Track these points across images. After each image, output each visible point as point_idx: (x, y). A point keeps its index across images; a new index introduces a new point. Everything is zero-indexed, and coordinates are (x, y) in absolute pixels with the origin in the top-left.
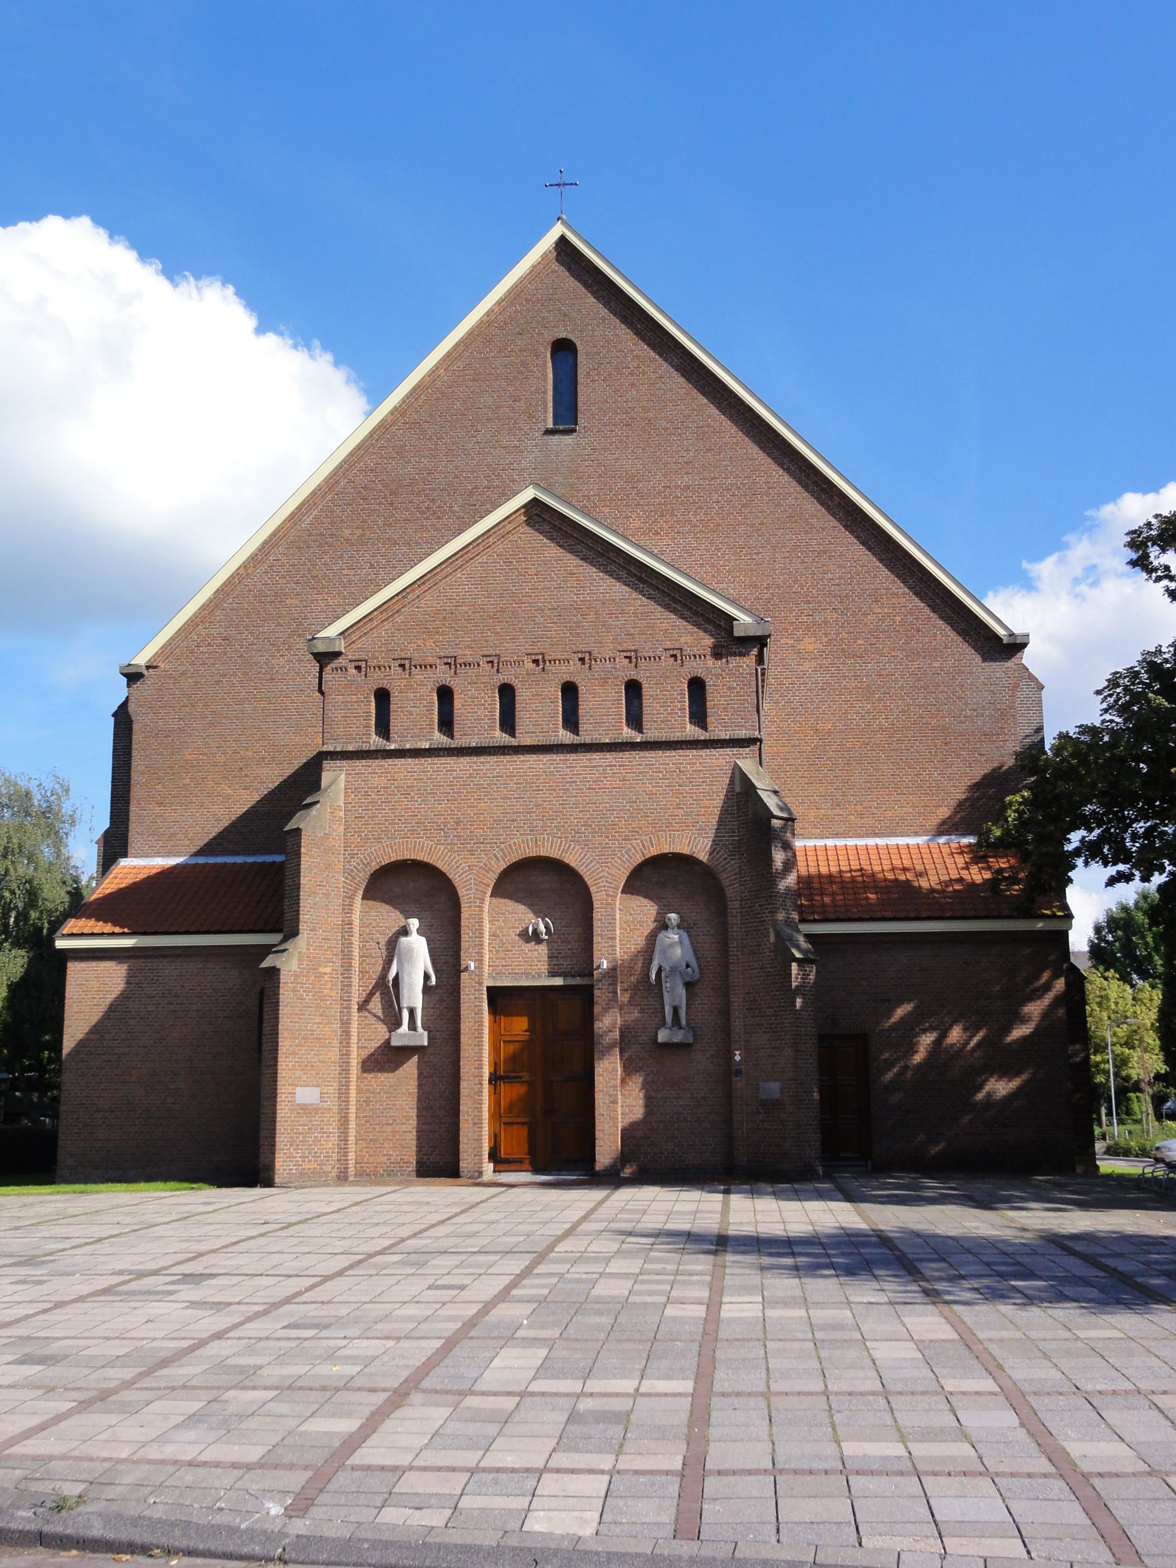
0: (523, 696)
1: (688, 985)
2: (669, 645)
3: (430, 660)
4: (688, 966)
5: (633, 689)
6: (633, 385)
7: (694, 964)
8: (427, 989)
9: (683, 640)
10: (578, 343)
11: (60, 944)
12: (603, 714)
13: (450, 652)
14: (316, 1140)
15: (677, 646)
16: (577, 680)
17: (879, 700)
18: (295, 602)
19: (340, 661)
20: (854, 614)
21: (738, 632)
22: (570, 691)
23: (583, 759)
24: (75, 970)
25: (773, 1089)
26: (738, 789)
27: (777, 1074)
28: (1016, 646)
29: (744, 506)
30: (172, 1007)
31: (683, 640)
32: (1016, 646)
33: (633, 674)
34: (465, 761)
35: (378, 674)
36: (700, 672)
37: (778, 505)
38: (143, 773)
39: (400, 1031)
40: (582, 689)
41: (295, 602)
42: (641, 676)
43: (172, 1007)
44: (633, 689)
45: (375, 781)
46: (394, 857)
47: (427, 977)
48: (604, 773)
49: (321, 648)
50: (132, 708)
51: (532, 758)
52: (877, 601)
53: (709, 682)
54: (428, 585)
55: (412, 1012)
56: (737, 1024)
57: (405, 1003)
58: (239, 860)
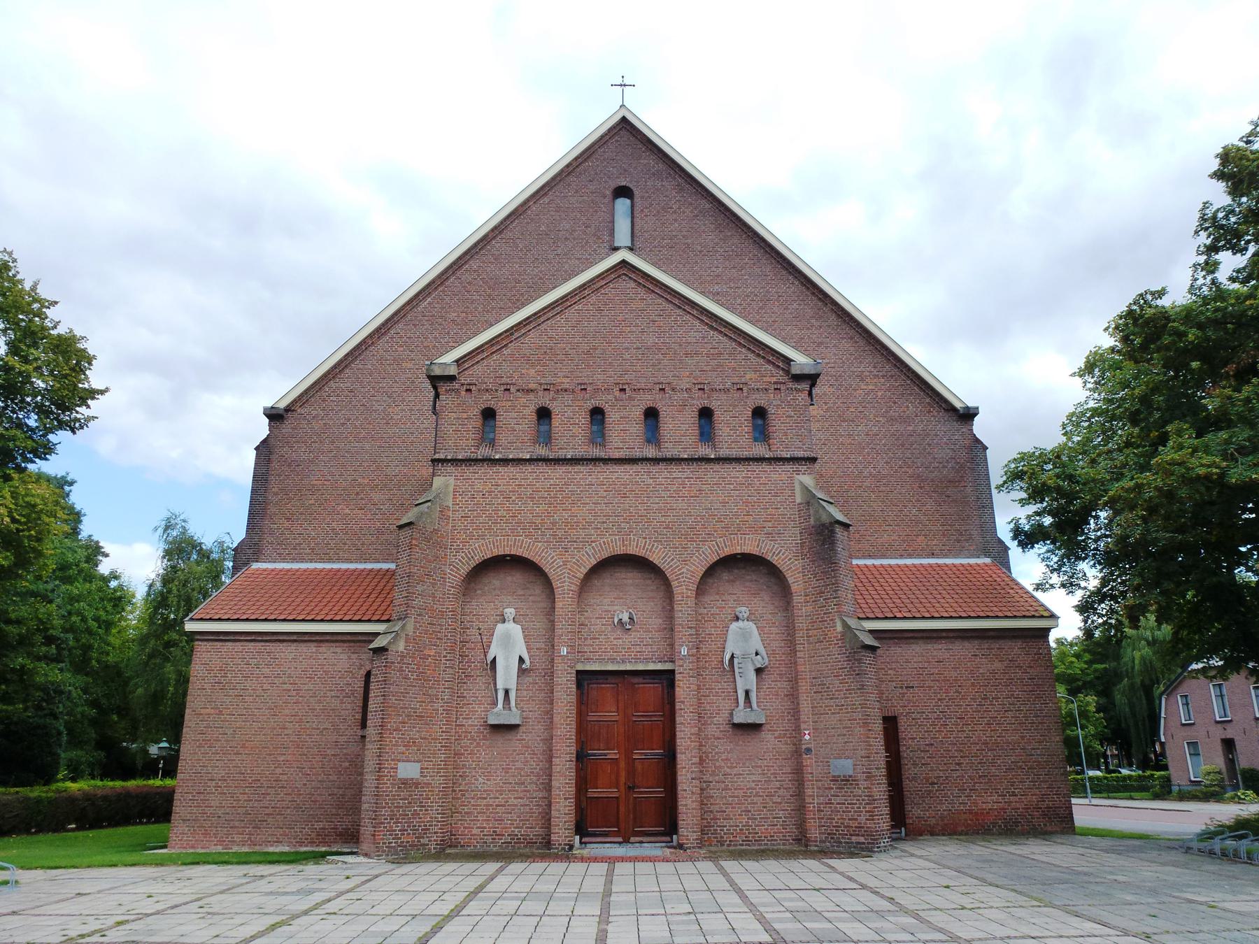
0: (612, 416)
1: (759, 671)
2: (736, 380)
3: (532, 386)
4: (757, 654)
5: (706, 414)
6: (676, 220)
7: (762, 651)
8: (522, 672)
9: (748, 376)
10: (635, 190)
11: (190, 627)
12: (679, 430)
13: (549, 379)
14: (415, 814)
15: (743, 380)
16: (659, 406)
17: (868, 454)
18: (410, 365)
19: (456, 385)
20: (847, 389)
21: (795, 370)
22: (651, 414)
23: (663, 473)
24: (203, 650)
25: (845, 766)
26: (798, 500)
27: (852, 756)
28: (968, 415)
29: (761, 308)
30: (285, 686)
31: (748, 376)
32: (968, 415)
33: (706, 403)
34: (560, 470)
35: (487, 396)
36: (763, 403)
37: (787, 309)
38: (276, 494)
39: (495, 710)
40: (662, 414)
41: (410, 365)
42: (714, 405)
43: (285, 686)
44: (706, 414)
45: (479, 486)
46: (496, 552)
47: (521, 660)
48: (683, 484)
49: (437, 371)
50: (272, 441)
51: (620, 469)
52: (862, 380)
53: (771, 410)
54: (532, 325)
55: (507, 692)
56: (805, 706)
57: (500, 685)
58: (352, 566)
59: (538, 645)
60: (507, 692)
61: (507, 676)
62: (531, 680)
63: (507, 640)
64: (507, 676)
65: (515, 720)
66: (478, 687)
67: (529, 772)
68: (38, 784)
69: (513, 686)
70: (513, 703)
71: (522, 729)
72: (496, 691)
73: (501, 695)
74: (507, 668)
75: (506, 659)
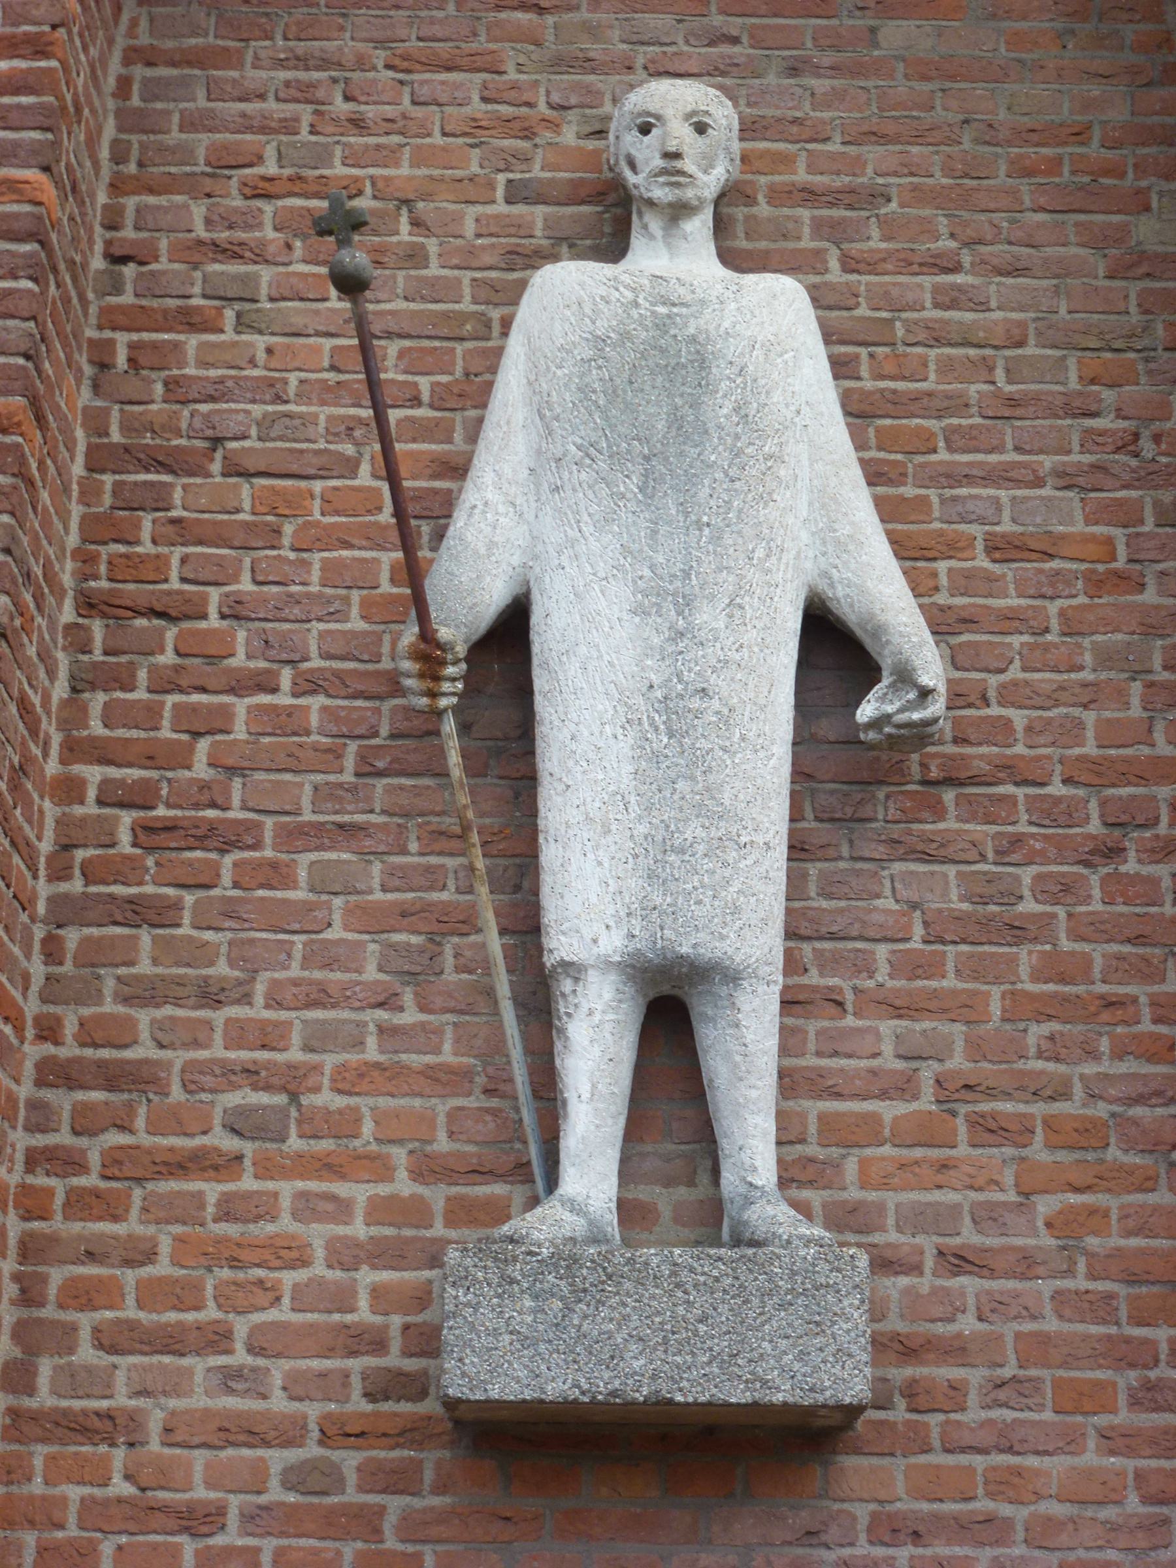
47: (833, 648)
55: (670, 1013)
57: (591, 909)
59: (1009, 511)
60: (670, 1013)
61: (659, 820)
62: (949, 890)
63: (662, 416)
64: (659, 820)
65: (811, 1358)
66: (306, 964)
67: (642, 1193)
68: (359, 1479)
69: (743, 917)
70: (752, 1144)
71: (869, 1481)
72: (539, 997)
73: (596, 1050)
74: (675, 717)
75: (670, 601)
